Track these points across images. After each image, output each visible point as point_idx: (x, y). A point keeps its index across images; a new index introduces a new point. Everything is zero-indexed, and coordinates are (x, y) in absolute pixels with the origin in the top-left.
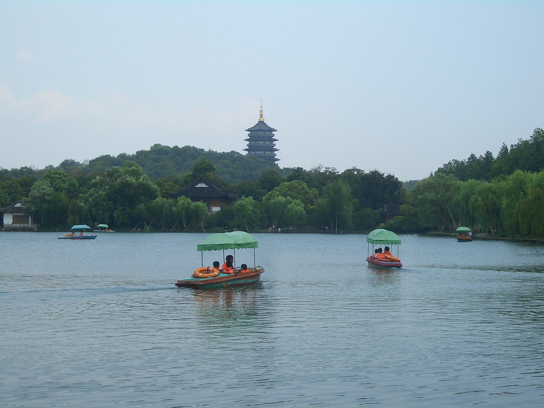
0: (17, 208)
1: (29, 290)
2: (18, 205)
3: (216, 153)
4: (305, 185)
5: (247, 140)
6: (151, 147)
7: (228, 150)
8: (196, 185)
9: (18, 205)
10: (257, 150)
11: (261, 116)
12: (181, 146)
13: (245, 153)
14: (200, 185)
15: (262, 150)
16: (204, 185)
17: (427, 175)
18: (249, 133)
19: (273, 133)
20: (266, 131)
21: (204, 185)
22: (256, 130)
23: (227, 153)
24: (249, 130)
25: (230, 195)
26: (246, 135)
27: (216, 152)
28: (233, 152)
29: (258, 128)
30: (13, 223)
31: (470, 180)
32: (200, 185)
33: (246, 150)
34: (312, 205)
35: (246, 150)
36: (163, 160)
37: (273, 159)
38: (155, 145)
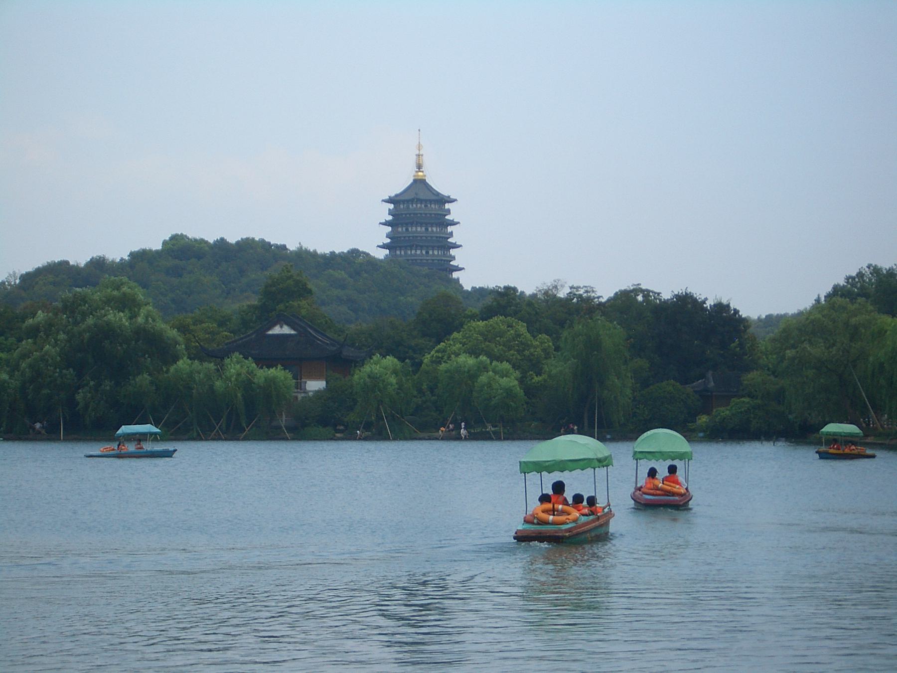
3: (314, 255)
4: (522, 327)
5: (387, 223)
7: (341, 247)
8: (269, 329)
11: (419, 167)
12: (232, 239)
13: (381, 254)
14: (277, 330)
16: (286, 330)
20: (431, 201)
21: (286, 330)
22: (408, 201)
24: (390, 201)
25: (348, 352)
26: (384, 212)
28: (355, 252)
29: (406, 197)
32: (277, 330)
33: (384, 246)
34: (539, 374)
35: (384, 246)
37: (446, 268)
38: (174, 238)
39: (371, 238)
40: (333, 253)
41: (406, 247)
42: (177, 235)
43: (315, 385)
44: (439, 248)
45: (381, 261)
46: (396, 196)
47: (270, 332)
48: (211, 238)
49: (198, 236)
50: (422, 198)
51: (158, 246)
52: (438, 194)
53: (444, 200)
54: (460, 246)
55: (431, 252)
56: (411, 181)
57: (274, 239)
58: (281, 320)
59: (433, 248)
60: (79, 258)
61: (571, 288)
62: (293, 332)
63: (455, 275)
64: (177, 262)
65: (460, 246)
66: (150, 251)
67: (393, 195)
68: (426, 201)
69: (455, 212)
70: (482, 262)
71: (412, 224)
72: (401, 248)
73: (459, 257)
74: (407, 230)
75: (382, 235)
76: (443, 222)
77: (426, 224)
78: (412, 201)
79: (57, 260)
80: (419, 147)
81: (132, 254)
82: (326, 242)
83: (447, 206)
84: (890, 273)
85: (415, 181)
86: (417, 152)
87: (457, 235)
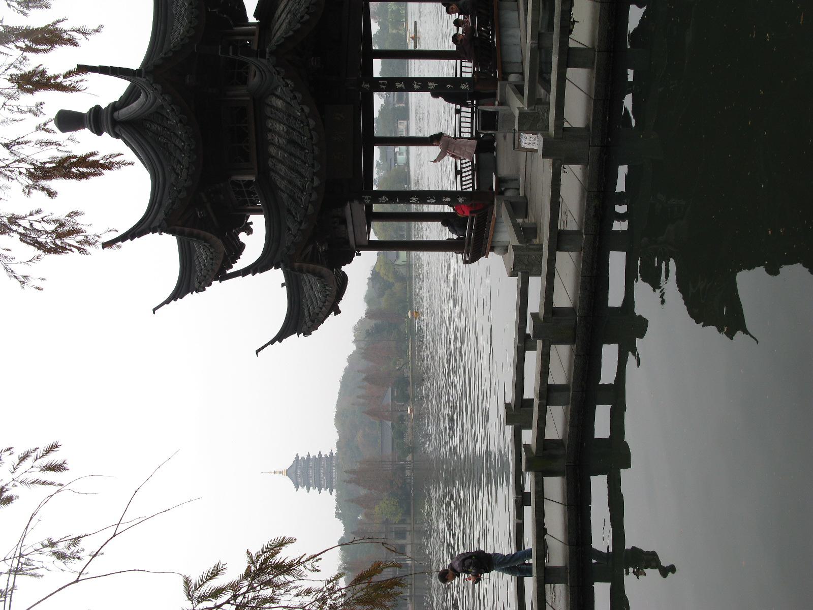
5: (320, 491)
11: (280, 473)
19: (323, 456)
20: (297, 465)
24: (297, 488)
26: (302, 490)
33: (331, 492)
69: (303, 455)
70: (324, 440)
73: (325, 452)
75: (325, 493)
78: (296, 474)
80: (270, 472)
87: (314, 453)
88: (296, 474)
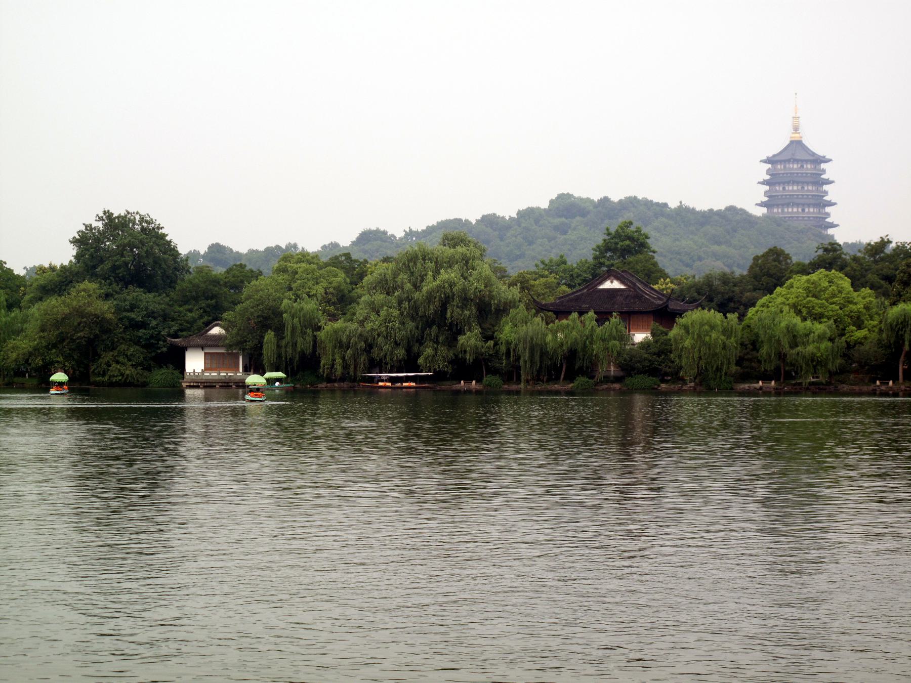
0: (214, 336)
1: (101, 543)
2: (216, 331)
3: (693, 211)
4: (846, 283)
5: (765, 183)
6: (551, 202)
7: (719, 205)
8: (601, 283)
9: (216, 331)
10: (788, 205)
11: (796, 129)
12: (615, 198)
13: (760, 212)
14: (607, 285)
15: (798, 205)
16: (617, 285)
17: (244, 250)
18: (769, 166)
20: (807, 161)
21: (617, 285)
22: (785, 161)
23: (719, 213)
24: (768, 161)
25: (673, 306)
26: (762, 172)
27: (606, 200)
28: (731, 209)
30: (206, 369)
31: (863, 289)
32: (607, 285)
33: (762, 204)
34: (859, 327)
35: (762, 204)
36: (575, 229)
37: (823, 224)
38: (561, 197)
39: (750, 198)
40: (711, 210)
41: (783, 205)
42: (563, 194)
43: (639, 337)
44: (815, 205)
45: (759, 218)
46: (774, 156)
47: (601, 287)
48: (596, 197)
49: (584, 196)
50: (798, 158)
51: (545, 205)
52: (814, 154)
53: (819, 160)
54: (835, 204)
55: (807, 210)
56: (788, 142)
57: (657, 198)
58: (611, 274)
59: (809, 205)
60: (739, 207)
61: (495, 270)
62: (622, 287)
63: (830, 231)
64: (563, 219)
65: (835, 204)
66: (539, 208)
67: (771, 155)
68: (802, 161)
69: (829, 171)
71: (788, 183)
72: (778, 206)
73: (834, 214)
74: (784, 188)
75: (760, 193)
76: (819, 181)
77: (803, 183)
79: (452, 217)
81: (519, 213)
82: (706, 198)
83: (823, 166)
84: (903, 252)
85: (792, 142)
86: (794, 115)
87: (832, 193)
88: (789, 161)
